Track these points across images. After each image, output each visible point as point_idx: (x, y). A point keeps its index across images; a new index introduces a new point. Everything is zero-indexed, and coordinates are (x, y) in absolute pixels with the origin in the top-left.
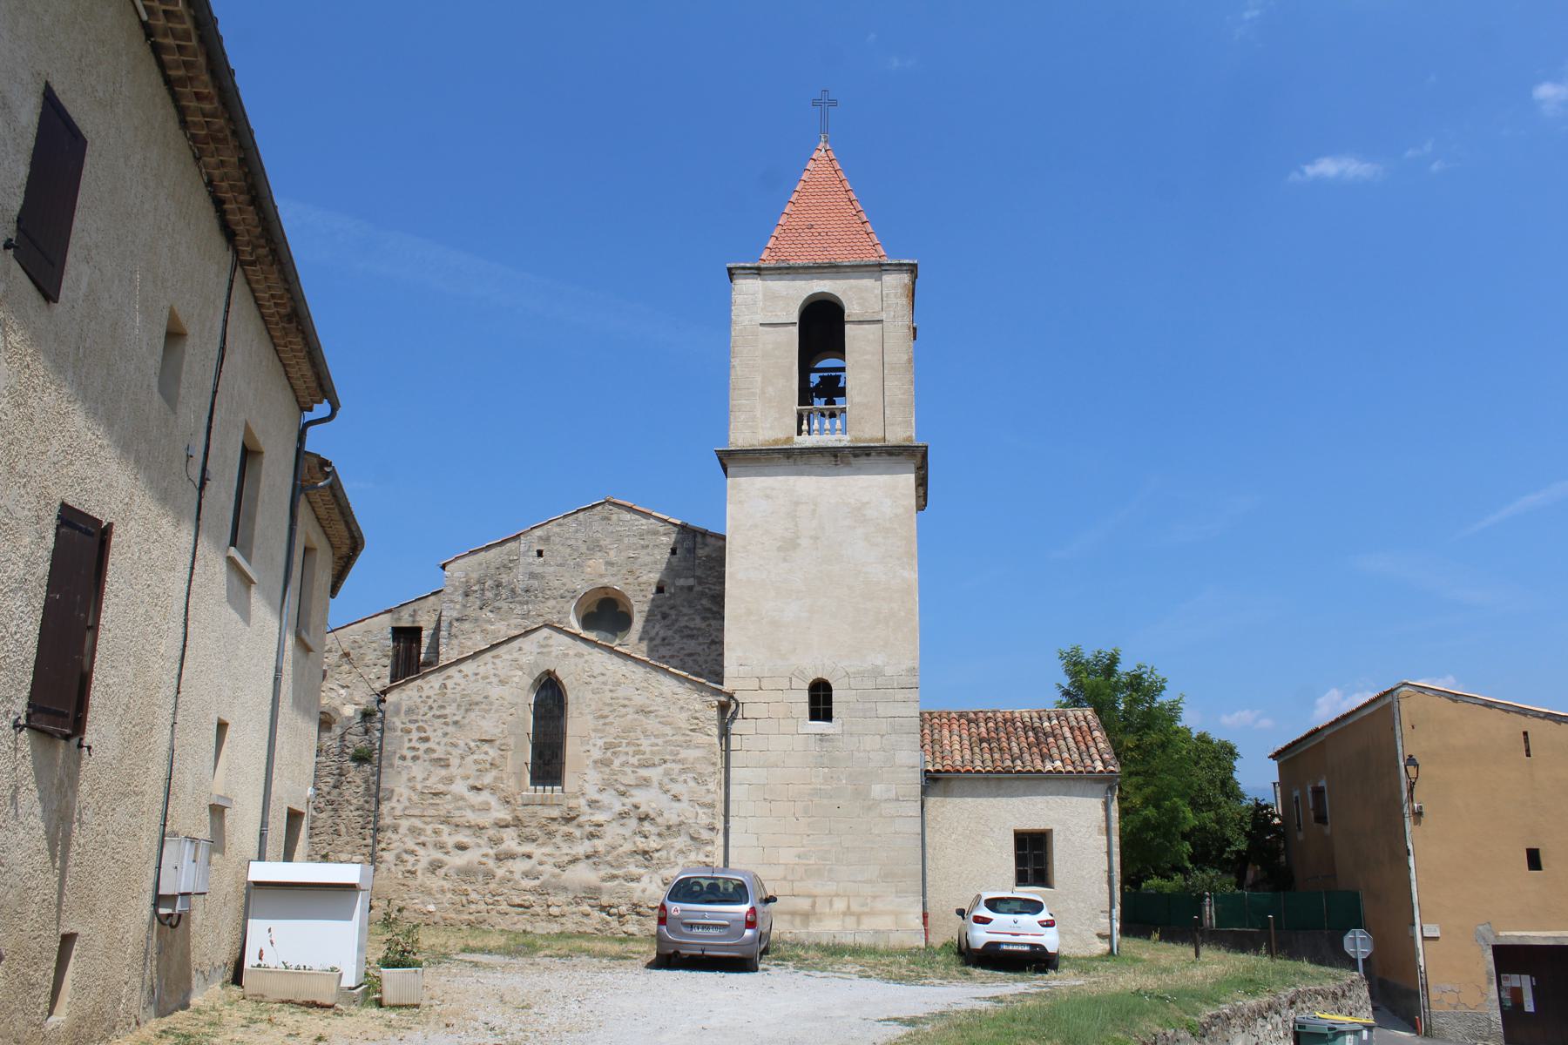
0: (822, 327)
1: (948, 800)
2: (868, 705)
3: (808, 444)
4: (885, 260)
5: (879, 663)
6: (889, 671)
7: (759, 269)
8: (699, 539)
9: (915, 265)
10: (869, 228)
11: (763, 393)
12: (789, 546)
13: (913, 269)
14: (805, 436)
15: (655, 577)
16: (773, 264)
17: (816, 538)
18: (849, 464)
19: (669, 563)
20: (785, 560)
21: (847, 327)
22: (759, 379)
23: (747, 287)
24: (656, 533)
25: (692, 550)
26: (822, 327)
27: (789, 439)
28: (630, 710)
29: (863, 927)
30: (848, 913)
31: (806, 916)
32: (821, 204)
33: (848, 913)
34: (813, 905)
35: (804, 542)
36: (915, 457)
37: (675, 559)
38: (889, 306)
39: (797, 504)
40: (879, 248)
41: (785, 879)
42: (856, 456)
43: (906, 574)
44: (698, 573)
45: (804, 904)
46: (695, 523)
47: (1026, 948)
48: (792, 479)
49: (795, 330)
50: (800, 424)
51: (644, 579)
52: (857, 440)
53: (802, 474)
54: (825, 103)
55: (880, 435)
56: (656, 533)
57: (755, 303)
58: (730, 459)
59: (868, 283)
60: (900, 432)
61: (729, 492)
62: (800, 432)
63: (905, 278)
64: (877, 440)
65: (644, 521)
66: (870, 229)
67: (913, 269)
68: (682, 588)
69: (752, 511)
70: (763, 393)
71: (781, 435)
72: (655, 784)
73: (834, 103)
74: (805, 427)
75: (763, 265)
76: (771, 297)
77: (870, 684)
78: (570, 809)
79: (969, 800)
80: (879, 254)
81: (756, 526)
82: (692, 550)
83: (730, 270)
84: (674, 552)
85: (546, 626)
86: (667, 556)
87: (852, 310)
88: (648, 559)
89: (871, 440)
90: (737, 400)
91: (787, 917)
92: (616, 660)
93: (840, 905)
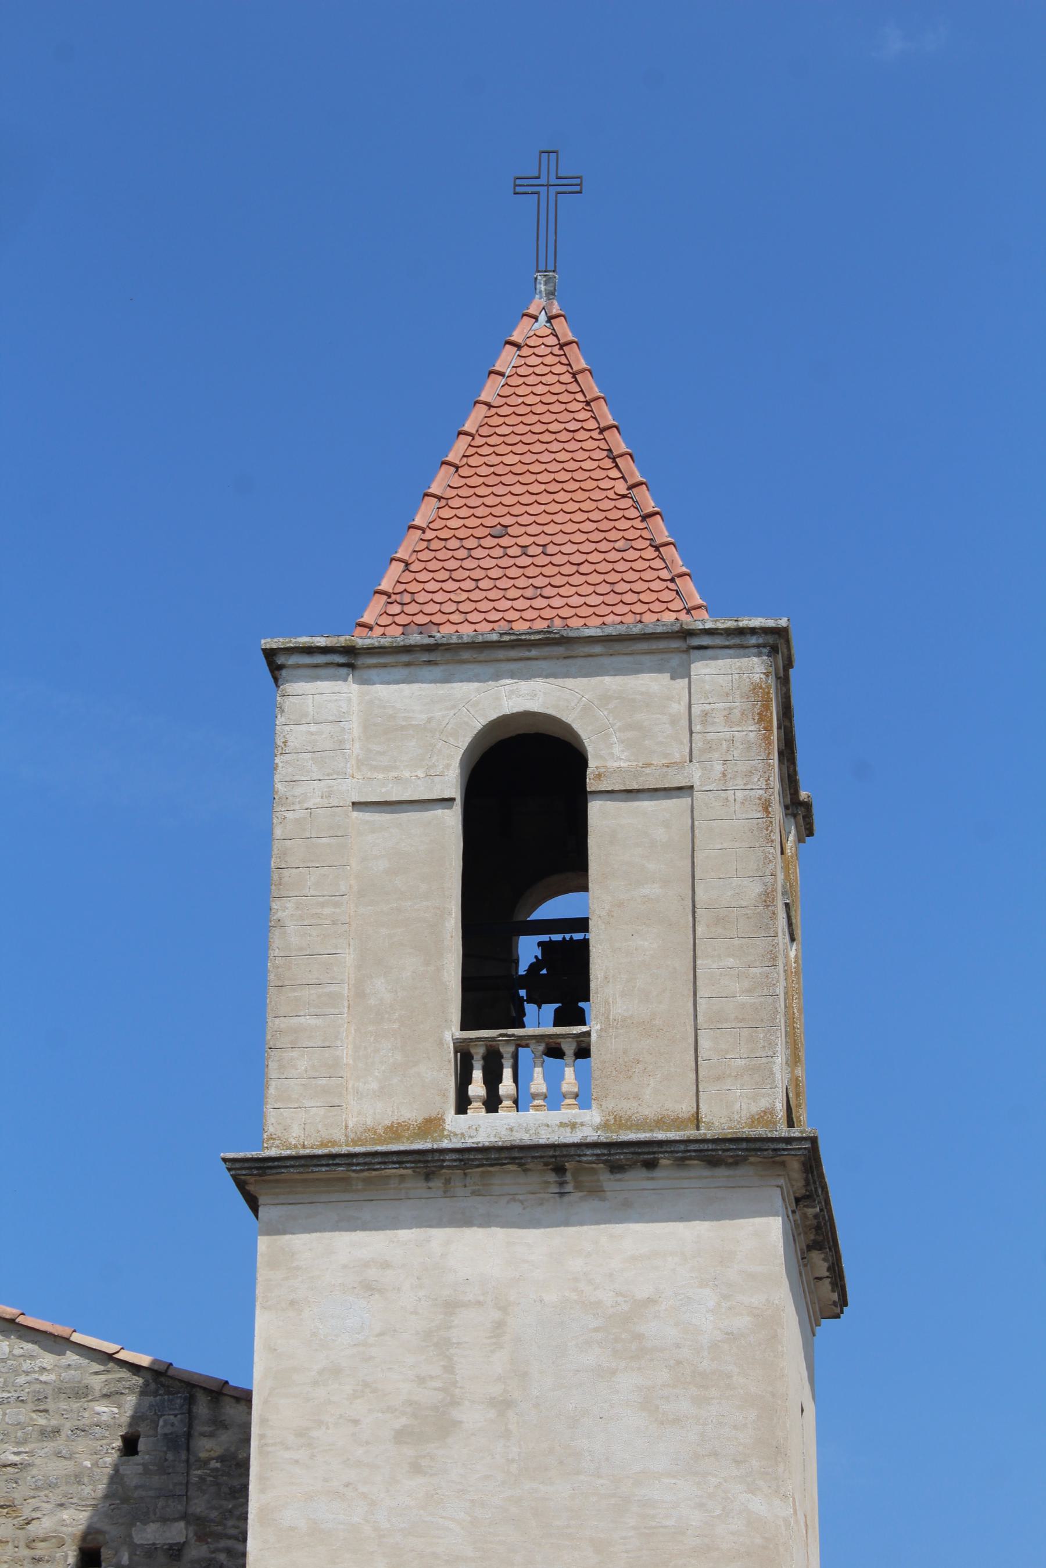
0: (525, 808)
3: (484, 1138)
4: (704, 620)
7: (350, 651)
8: (202, 1408)
9: (781, 633)
10: (661, 531)
11: (360, 994)
12: (428, 1426)
13: (776, 643)
14: (477, 1114)
15: (74, 1520)
16: (393, 636)
17: (503, 1404)
18: (596, 1191)
19: (116, 1477)
20: (416, 1469)
21: (595, 809)
22: (349, 957)
23: (320, 708)
24: (81, 1393)
25: (181, 1442)
26: (525, 808)
27: (432, 1124)
32: (529, 450)
35: (472, 1416)
36: (781, 1167)
37: (133, 1468)
38: (709, 747)
39: (451, 1306)
40: (687, 586)
42: (616, 1168)
44: (199, 1506)
46: (190, 1361)
48: (438, 1236)
49: (452, 819)
50: (464, 1080)
51: (45, 1525)
52: (620, 1122)
53: (466, 1222)
54: (548, 185)
55: (686, 1108)
56: (81, 1393)
57: (339, 747)
58: (264, 1180)
59: (652, 684)
60: (738, 1104)
61: (263, 1274)
62: (463, 1104)
63: (754, 668)
64: (678, 1123)
65: (48, 1359)
66: (663, 534)
67: (776, 643)
68: (151, 1551)
69: (326, 1323)
70: (360, 994)
71: (411, 1113)
73: (574, 186)
74: (477, 1088)
75: (361, 639)
76: (383, 729)
80: (694, 605)
81: (335, 1372)
82: (181, 1442)
83: (270, 654)
84: (130, 1446)
86: (111, 1458)
87: (607, 760)
88: (58, 1468)
89: (660, 1123)
90: (289, 1017)
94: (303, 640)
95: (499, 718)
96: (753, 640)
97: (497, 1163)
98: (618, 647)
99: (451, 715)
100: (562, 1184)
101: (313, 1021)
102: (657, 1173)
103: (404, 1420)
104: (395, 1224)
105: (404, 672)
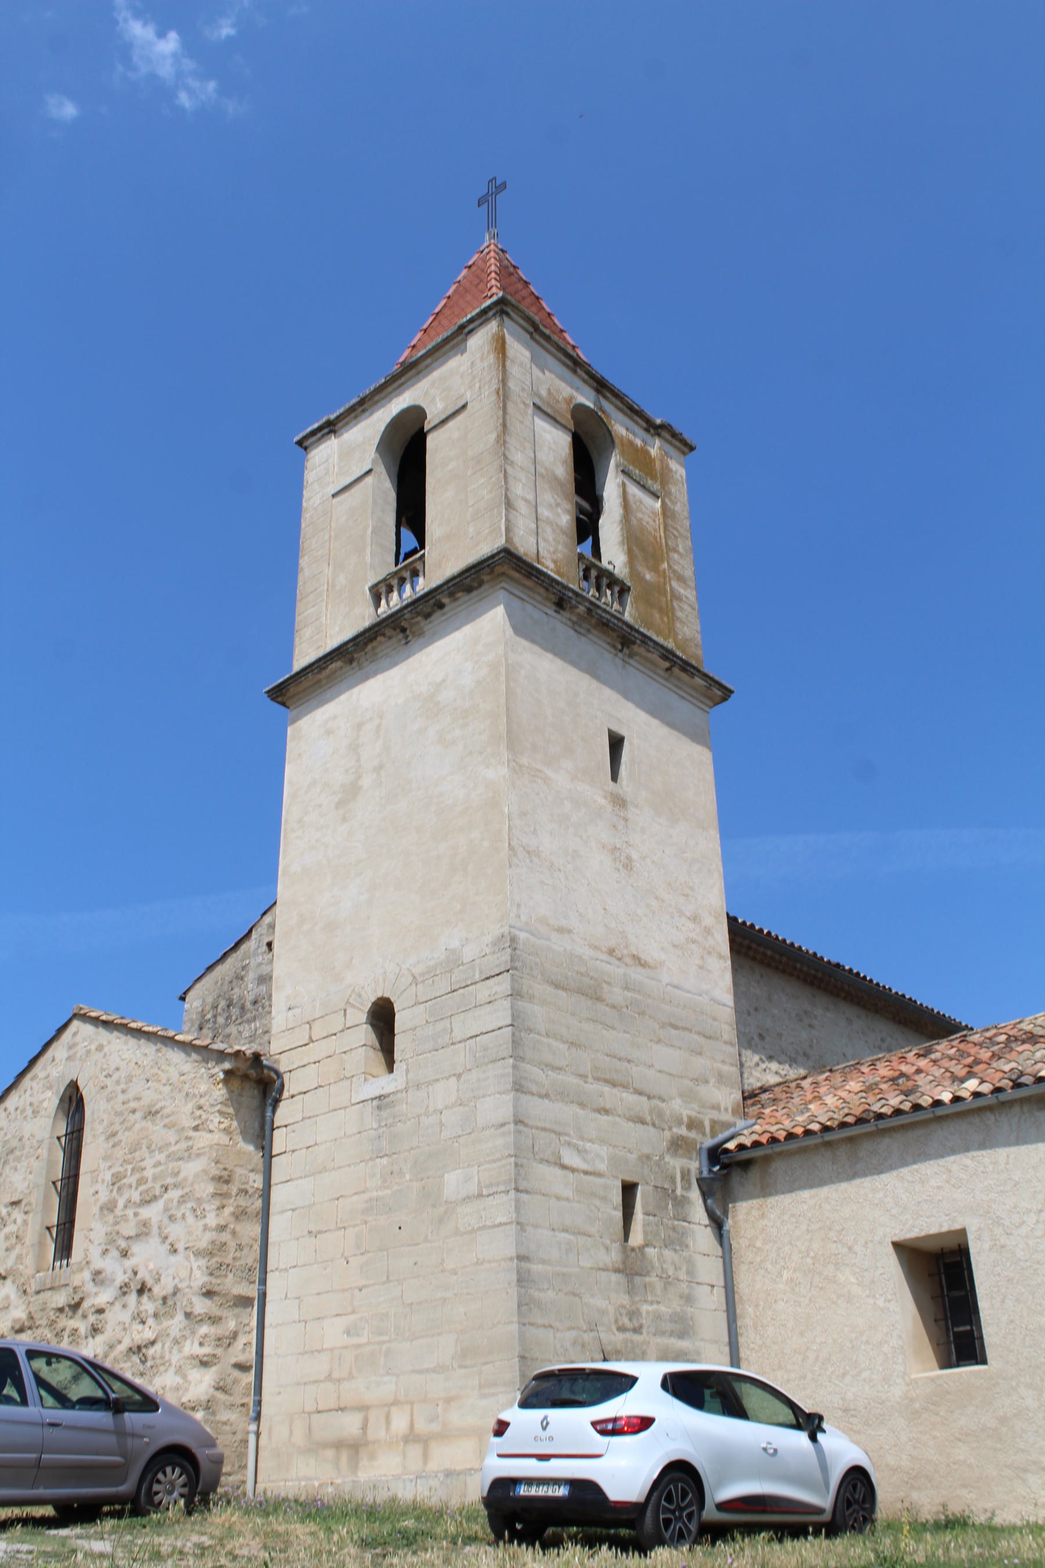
1: (771, 1200)
2: (440, 1026)
5: (455, 944)
6: (469, 953)
18: (421, 634)
28: (139, 1115)
29: (433, 1466)
30: (411, 1437)
31: (354, 1448)
33: (411, 1437)
34: (364, 1428)
41: (329, 1378)
43: (491, 774)
45: (350, 1424)
47: (562, 1492)
72: (155, 1230)
77: (443, 986)
78: (75, 1289)
79: (805, 1194)
83: (300, 443)
85: (75, 1016)
91: (330, 1453)
92: (132, 1042)
93: (400, 1423)
94: (310, 429)
95: (392, 420)
96: (491, 313)
97: (372, 639)
98: (437, 354)
99: (368, 432)
100: (407, 637)
101: (313, 609)
102: (446, 609)
103: (340, 796)
104: (339, 694)
105: (354, 422)
